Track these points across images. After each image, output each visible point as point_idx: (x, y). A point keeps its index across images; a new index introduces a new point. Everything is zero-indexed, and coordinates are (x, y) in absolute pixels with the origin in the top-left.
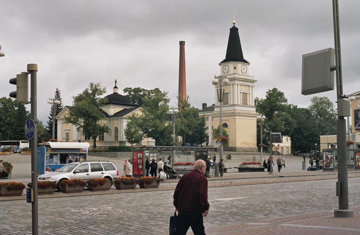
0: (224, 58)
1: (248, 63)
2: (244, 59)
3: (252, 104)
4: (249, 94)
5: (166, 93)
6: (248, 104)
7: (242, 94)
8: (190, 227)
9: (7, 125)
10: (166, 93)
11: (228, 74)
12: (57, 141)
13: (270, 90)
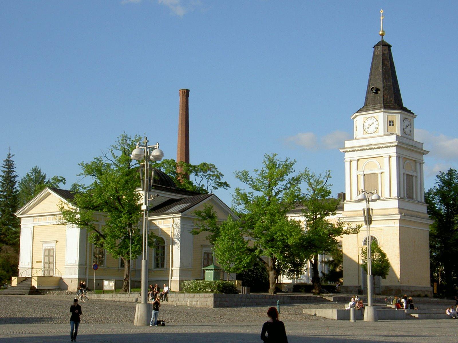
0: (362, 105)
1: (413, 114)
2: (404, 106)
3: (421, 199)
4: (416, 177)
6: (415, 198)
7: (405, 176)
8: (267, 332)
9: (74, 212)
10: (292, 164)
12: (182, 90)
13: (443, 173)
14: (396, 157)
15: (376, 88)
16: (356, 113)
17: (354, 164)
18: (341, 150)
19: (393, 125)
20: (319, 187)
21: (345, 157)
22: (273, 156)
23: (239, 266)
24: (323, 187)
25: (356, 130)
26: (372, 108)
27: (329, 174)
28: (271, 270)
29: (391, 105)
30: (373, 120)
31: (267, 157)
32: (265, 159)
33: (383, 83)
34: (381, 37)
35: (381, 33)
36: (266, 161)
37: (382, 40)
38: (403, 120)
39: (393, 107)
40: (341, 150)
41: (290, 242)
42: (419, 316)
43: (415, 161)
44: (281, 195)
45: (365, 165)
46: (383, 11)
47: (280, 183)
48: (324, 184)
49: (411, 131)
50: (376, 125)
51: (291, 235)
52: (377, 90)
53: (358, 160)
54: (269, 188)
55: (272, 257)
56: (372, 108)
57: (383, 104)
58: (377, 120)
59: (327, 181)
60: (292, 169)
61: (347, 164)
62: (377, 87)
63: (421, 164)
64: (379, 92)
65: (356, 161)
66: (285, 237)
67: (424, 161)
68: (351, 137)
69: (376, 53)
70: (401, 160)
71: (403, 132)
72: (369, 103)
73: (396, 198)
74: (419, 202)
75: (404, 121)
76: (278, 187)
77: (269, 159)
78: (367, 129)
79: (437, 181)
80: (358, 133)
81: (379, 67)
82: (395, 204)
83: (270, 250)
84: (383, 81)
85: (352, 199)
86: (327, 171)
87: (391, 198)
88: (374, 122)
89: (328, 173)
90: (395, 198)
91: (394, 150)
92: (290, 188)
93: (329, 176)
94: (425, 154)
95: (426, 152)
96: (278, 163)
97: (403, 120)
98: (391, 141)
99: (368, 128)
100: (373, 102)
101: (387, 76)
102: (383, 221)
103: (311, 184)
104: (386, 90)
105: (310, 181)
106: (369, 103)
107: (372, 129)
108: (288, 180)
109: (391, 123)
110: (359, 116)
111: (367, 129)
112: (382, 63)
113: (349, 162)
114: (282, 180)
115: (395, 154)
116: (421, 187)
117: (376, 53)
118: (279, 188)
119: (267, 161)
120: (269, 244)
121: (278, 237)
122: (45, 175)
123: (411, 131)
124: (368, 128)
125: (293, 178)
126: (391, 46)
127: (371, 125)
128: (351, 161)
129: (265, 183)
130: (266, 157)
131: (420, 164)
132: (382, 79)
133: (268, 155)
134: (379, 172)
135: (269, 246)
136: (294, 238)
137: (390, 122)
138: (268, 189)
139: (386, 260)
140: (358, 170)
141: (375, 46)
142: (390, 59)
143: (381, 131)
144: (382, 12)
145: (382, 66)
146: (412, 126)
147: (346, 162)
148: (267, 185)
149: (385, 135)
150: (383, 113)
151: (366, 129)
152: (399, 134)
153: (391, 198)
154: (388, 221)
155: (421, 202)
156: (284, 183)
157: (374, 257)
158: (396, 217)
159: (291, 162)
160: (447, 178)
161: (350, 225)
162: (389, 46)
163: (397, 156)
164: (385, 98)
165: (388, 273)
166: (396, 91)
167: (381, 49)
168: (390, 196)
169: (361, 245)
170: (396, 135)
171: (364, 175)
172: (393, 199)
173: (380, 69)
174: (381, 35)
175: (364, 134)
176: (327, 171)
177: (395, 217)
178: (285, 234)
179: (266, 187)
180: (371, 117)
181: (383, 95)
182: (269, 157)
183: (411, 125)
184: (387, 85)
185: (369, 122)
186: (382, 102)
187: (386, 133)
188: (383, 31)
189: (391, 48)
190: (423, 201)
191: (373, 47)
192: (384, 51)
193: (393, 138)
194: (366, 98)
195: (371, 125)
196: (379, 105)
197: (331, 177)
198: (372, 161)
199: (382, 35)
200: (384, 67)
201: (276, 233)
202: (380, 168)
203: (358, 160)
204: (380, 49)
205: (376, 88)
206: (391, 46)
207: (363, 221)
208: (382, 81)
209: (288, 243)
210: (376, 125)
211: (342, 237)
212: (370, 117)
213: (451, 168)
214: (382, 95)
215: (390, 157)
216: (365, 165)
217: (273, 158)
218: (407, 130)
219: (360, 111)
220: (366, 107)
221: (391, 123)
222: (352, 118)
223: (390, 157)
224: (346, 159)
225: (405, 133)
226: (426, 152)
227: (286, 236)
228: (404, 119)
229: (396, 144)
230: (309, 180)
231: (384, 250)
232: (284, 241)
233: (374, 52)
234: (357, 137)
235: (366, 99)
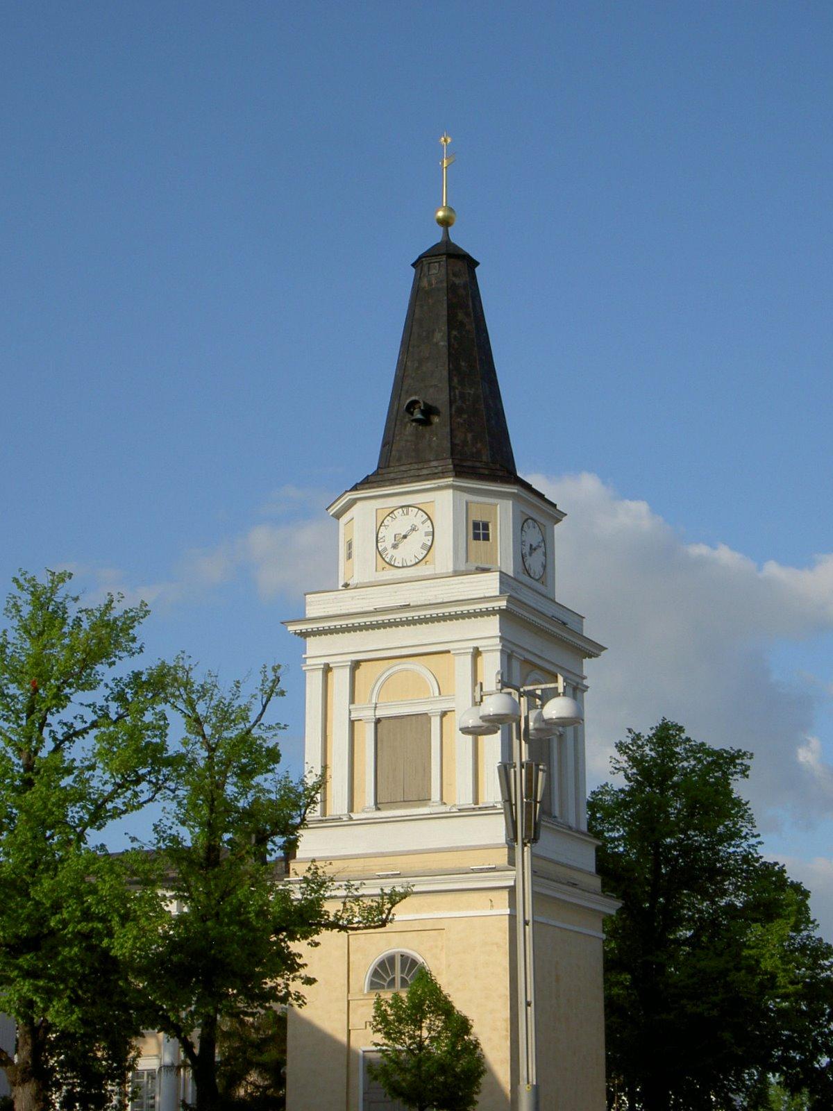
5: (131, 620)
10: (131, 620)
11: (422, 570)
13: (638, 736)
14: (498, 654)
15: (425, 404)
16: (352, 490)
17: (340, 679)
18: (291, 628)
19: (486, 537)
20: (232, 734)
22: (53, 581)
24: (249, 732)
25: (349, 556)
26: (412, 473)
27: (277, 680)
28: (24, 1081)
29: (478, 464)
30: (416, 518)
31: (26, 585)
32: (17, 592)
33: (451, 388)
34: (441, 229)
35: (440, 214)
36: (19, 603)
37: (445, 239)
38: (523, 522)
39: (487, 472)
41: (122, 946)
44: (79, 751)
45: (379, 684)
46: (449, 140)
47: (79, 697)
48: (253, 718)
49: (544, 567)
50: (427, 534)
51: (125, 918)
52: (429, 411)
53: (356, 665)
54: (28, 717)
55: (29, 1021)
56: (412, 473)
57: (450, 461)
58: (429, 518)
59: (264, 707)
60: (134, 640)
61: (314, 682)
62: (430, 403)
64: (436, 420)
65: (348, 670)
66: (100, 926)
67: (585, 682)
68: (305, 653)
69: (425, 283)
70: (516, 665)
71: (520, 569)
72: (399, 460)
73: (499, 806)
74: (570, 828)
75: (525, 529)
76: (67, 714)
77: (32, 593)
78: (391, 552)
79: (618, 762)
80: (361, 567)
81: (434, 331)
83: (25, 987)
84: (450, 380)
85: (484, 690)
86: (269, 669)
87: (480, 809)
88: (420, 526)
89: (271, 676)
90: (494, 807)
91: (492, 626)
92: (121, 717)
93: (274, 686)
94: (590, 656)
96: (72, 612)
97: (523, 523)
99: (395, 546)
100: (413, 454)
101: (463, 364)
102: (450, 897)
103: (197, 720)
104: (460, 411)
105: (194, 710)
106: (399, 460)
107: (411, 550)
108: (112, 685)
109: (480, 531)
110: (359, 505)
111: (391, 552)
112: (445, 318)
113: (320, 674)
114: (90, 686)
115: (496, 643)
116: (576, 769)
117: (425, 283)
118: (70, 720)
119: (26, 602)
120: (21, 961)
121: (65, 923)
123: (544, 567)
124: (395, 546)
125: (137, 675)
126: (477, 264)
127: (405, 537)
128: (327, 669)
129: (13, 697)
130: (20, 587)
132: (445, 373)
133: (28, 576)
134: (434, 708)
135: (19, 968)
136: (142, 929)
137: (476, 525)
138: (24, 722)
139: (470, 1042)
140: (352, 701)
141: (420, 258)
142: (474, 304)
143: (444, 557)
144: (446, 141)
145: (445, 328)
146: (548, 549)
147: (308, 674)
148: (19, 706)
149: (456, 573)
150: (451, 491)
151: (385, 549)
152: (510, 571)
153: (480, 809)
154: (466, 896)
155: (578, 831)
156: (98, 696)
157: (425, 1034)
158: (499, 878)
159: (126, 612)
160: (653, 754)
161: (356, 889)
162: (472, 264)
163: (502, 651)
164: (457, 441)
165: (476, 1097)
166: (493, 422)
167: (443, 270)
168: (476, 801)
169: (361, 990)
170: (501, 572)
171: (378, 721)
172: (487, 810)
173: (440, 338)
175: (380, 568)
176: (269, 669)
177: (494, 879)
178: (101, 910)
179: (17, 712)
180: (409, 506)
181: (452, 430)
182: (34, 586)
183: (545, 546)
184: (462, 396)
185: (400, 524)
186: (447, 454)
187: (462, 568)
189: (477, 270)
190: (584, 827)
191: (413, 265)
192: (455, 275)
193: (489, 585)
194: (387, 443)
195: (405, 537)
196: (434, 464)
197: (282, 693)
198: (407, 670)
199: (445, 223)
200: (454, 333)
201: (57, 907)
203: (356, 665)
204: (437, 271)
205: (425, 404)
206: (477, 264)
207: (502, 813)
208: (447, 379)
209: (112, 953)
210: (427, 534)
211: (317, 944)
212: (402, 507)
213: (664, 719)
214: (448, 429)
215: (477, 653)
216: (379, 684)
217: (53, 590)
218: (535, 562)
219: (367, 483)
220: (384, 471)
221: (480, 531)
222: (333, 510)
223: (477, 653)
224: (309, 662)
225: (527, 571)
227: (103, 919)
228: (527, 519)
229: (503, 604)
230: (191, 704)
231: (461, 1005)
232: (94, 942)
233: (417, 280)
234: (352, 582)
235: (384, 446)
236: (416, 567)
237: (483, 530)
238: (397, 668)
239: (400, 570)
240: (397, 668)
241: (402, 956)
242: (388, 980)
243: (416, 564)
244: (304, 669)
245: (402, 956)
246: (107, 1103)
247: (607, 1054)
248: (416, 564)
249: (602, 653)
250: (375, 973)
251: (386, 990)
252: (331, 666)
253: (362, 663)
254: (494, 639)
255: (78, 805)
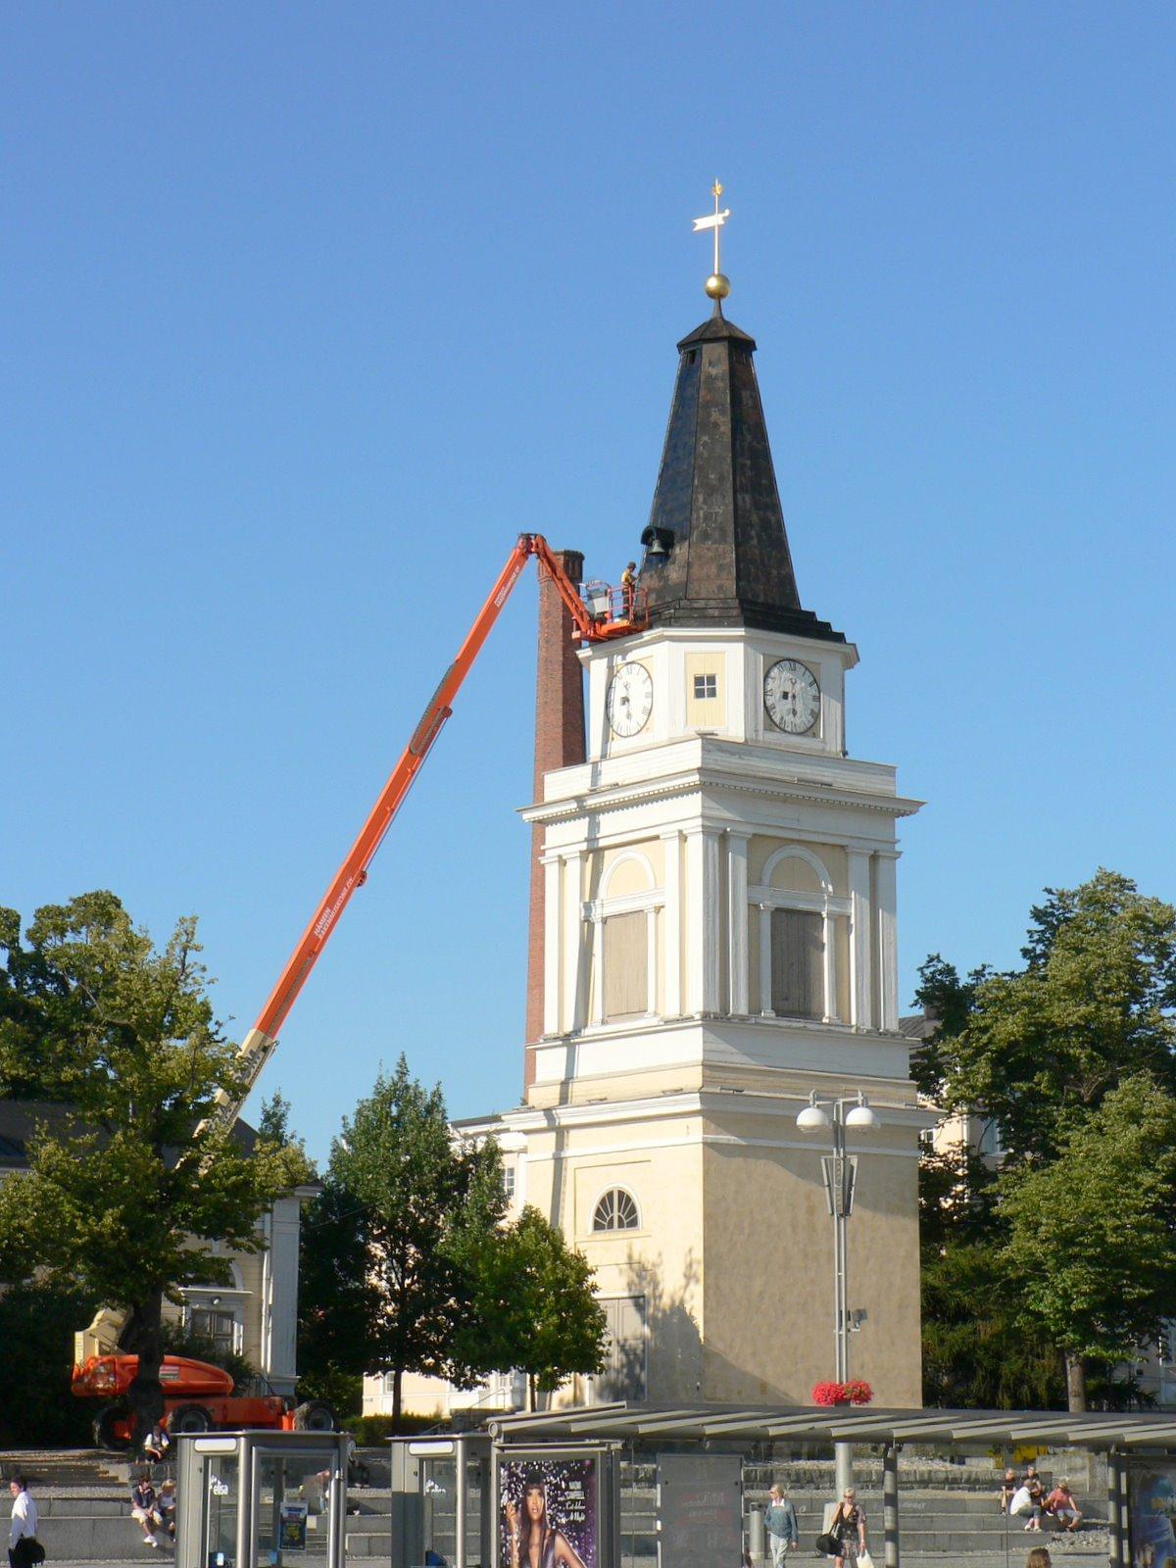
1: (839, 638)
18: (528, 816)
21: (544, 843)
23: (316, 1379)
27: (190, 934)
35: (713, 283)
40: (528, 816)
42: (318, 1524)
43: (843, 847)
63: (883, 864)
82: (691, 1045)
91: (694, 803)
95: (910, 808)
98: (686, 769)
109: (705, 686)
122: (970, 975)
131: (874, 858)
137: (699, 681)
150: (741, 645)
174: (712, 295)
188: (723, 279)
199: (717, 295)
202: (653, 886)
212: (789, 660)
215: (683, 837)
221: (705, 686)
224: (548, 853)
226: (910, 808)
236: (639, 735)
237: (708, 684)
238: (624, 856)
239: (627, 739)
240: (624, 856)
241: (619, 1192)
242: (608, 1219)
243: (639, 732)
244: (542, 862)
245: (619, 1192)
246: (232, 1351)
247: (299, 1323)
248: (639, 732)
249: (921, 808)
250: (598, 1213)
251: (606, 1230)
252: (685, 832)
253: (606, 852)
254: (697, 820)
255: (1073, 915)
